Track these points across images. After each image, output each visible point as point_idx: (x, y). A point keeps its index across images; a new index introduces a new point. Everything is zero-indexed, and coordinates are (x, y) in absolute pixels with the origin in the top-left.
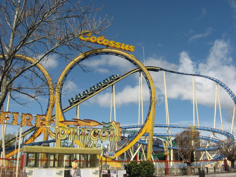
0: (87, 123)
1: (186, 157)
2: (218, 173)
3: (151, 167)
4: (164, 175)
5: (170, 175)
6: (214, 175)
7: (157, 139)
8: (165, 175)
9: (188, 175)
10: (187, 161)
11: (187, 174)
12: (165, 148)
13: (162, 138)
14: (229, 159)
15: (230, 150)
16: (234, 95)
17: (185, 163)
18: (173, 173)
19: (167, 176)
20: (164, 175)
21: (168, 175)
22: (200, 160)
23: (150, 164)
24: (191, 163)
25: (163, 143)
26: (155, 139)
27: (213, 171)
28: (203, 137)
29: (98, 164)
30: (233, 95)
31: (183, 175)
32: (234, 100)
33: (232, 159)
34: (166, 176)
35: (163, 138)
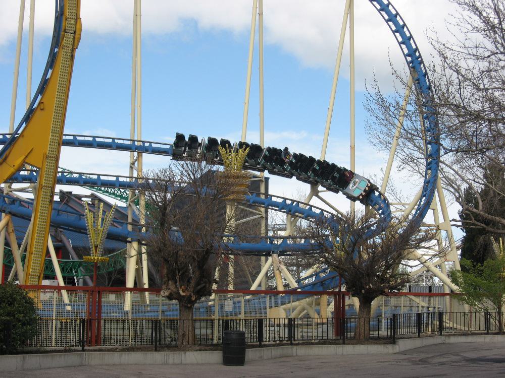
0: (49, 194)
1: (178, 277)
2: (307, 343)
3: (20, 312)
4: (76, 348)
5: (103, 347)
6: (288, 350)
7: (93, 197)
8: (80, 348)
9: (180, 350)
10: (181, 292)
11: (97, 343)
12: (90, 231)
13: (114, 194)
14: (354, 290)
15: (360, 256)
16: (398, 17)
17: (170, 297)
18: (120, 338)
19: (89, 350)
20: (76, 348)
21: (97, 347)
22: (254, 287)
23: (15, 300)
24: (195, 302)
25: (87, 211)
26: (86, 197)
27: (285, 333)
28: (136, 143)
29: (34, 318)
30: (403, 28)
31: (156, 350)
32: (409, 59)
33: (363, 291)
34: (83, 350)
35: (110, 194)
